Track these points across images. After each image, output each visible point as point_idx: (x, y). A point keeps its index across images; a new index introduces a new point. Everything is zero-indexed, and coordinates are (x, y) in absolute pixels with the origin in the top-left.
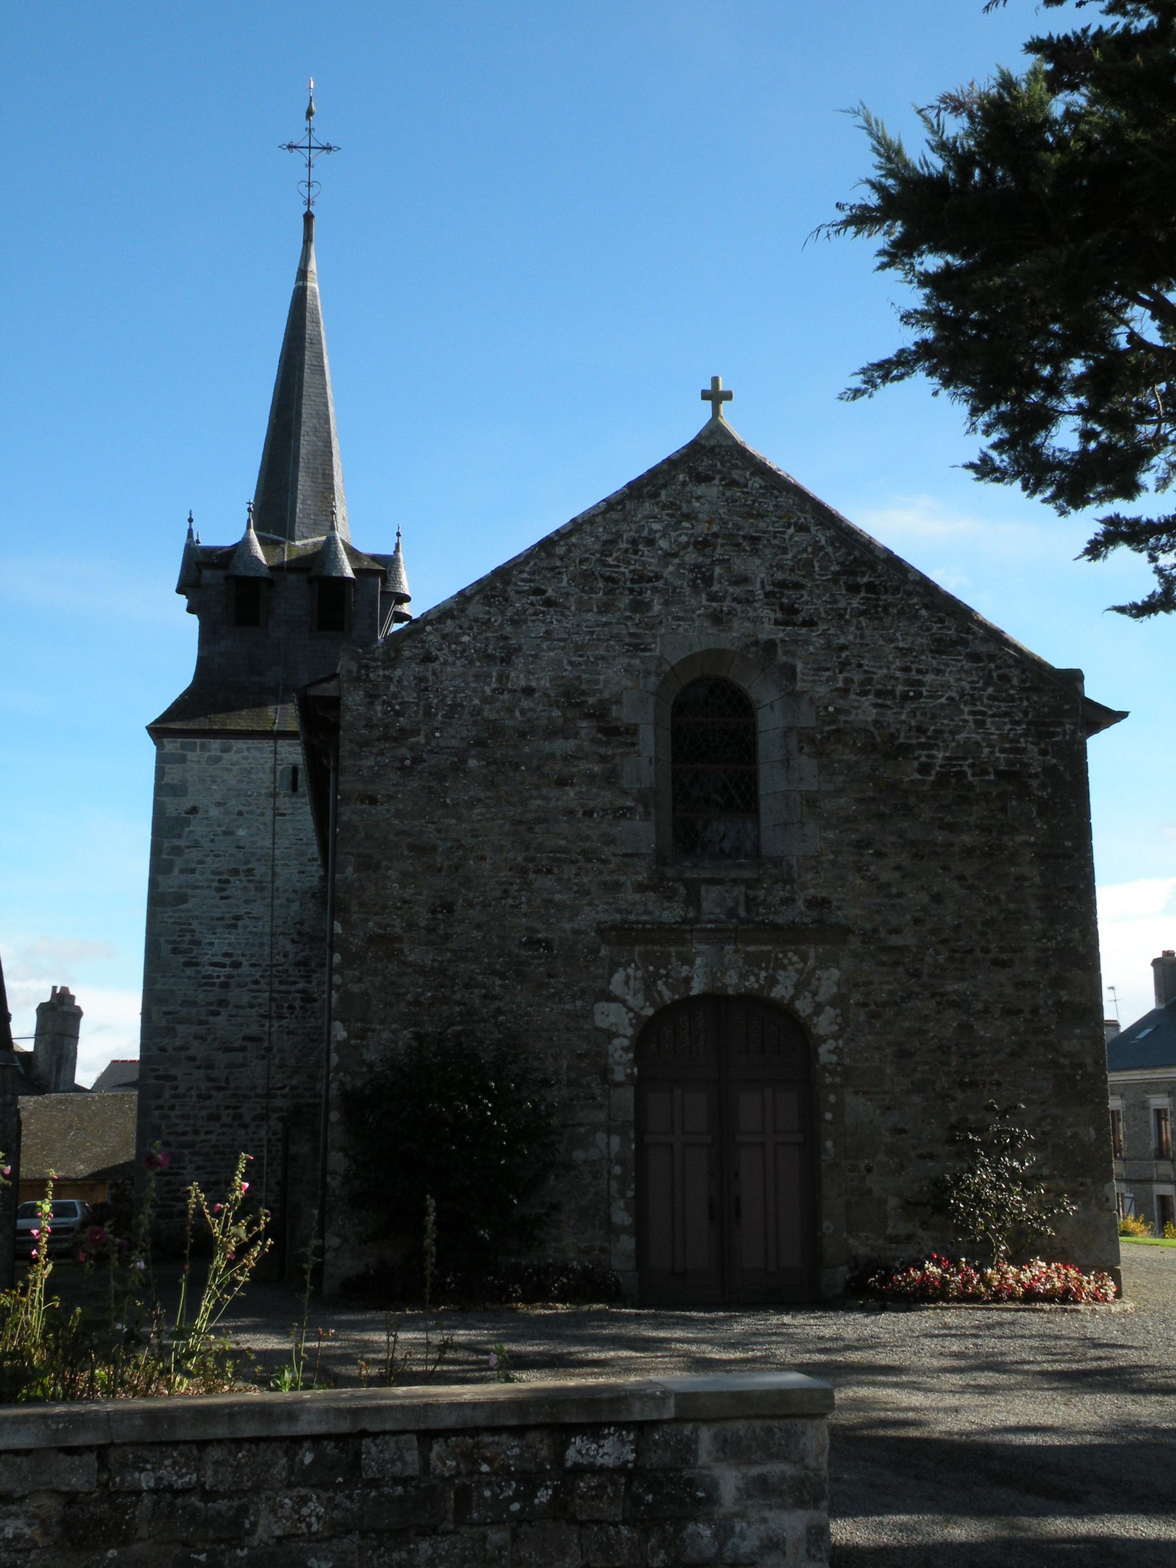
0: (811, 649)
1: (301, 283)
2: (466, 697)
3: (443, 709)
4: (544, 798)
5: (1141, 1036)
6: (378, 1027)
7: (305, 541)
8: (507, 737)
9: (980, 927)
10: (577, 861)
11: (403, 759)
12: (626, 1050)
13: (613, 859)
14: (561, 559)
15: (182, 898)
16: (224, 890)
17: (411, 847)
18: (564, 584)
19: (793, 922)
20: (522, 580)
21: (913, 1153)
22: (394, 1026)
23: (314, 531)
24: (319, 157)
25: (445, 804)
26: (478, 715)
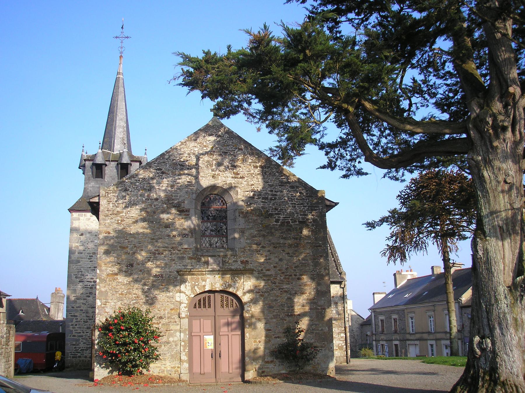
0: (243, 185)
4: (161, 232)
5: (424, 294)
6: (110, 301)
9: (294, 268)
10: (171, 251)
12: (185, 307)
13: (182, 250)
15: (78, 262)
16: (91, 259)
17: (120, 247)
18: (168, 167)
19: (237, 268)
21: (273, 337)
22: (115, 301)
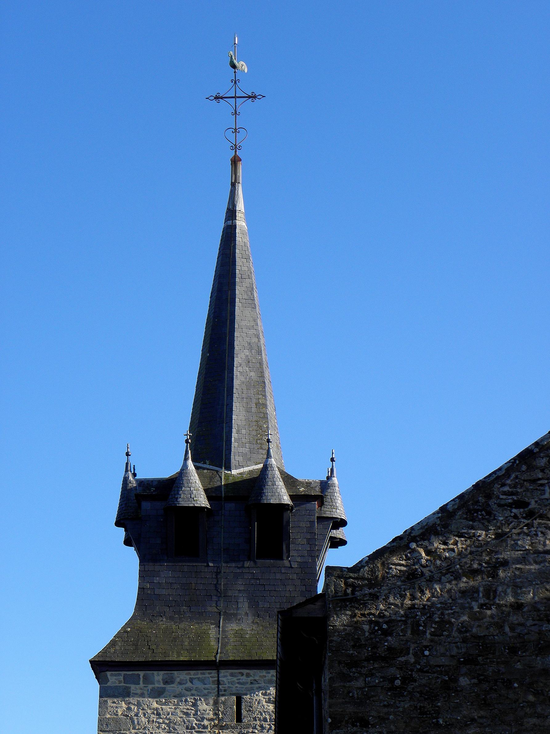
1: (230, 223)
2: (453, 614)
3: (432, 627)
7: (241, 470)
8: (497, 654)
11: (392, 680)
14: (542, 471)
20: (504, 493)
23: (248, 461)
24: (245, 106)
25: (437, 725)
26: (466, 631)
